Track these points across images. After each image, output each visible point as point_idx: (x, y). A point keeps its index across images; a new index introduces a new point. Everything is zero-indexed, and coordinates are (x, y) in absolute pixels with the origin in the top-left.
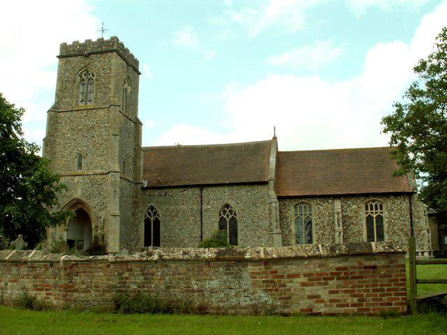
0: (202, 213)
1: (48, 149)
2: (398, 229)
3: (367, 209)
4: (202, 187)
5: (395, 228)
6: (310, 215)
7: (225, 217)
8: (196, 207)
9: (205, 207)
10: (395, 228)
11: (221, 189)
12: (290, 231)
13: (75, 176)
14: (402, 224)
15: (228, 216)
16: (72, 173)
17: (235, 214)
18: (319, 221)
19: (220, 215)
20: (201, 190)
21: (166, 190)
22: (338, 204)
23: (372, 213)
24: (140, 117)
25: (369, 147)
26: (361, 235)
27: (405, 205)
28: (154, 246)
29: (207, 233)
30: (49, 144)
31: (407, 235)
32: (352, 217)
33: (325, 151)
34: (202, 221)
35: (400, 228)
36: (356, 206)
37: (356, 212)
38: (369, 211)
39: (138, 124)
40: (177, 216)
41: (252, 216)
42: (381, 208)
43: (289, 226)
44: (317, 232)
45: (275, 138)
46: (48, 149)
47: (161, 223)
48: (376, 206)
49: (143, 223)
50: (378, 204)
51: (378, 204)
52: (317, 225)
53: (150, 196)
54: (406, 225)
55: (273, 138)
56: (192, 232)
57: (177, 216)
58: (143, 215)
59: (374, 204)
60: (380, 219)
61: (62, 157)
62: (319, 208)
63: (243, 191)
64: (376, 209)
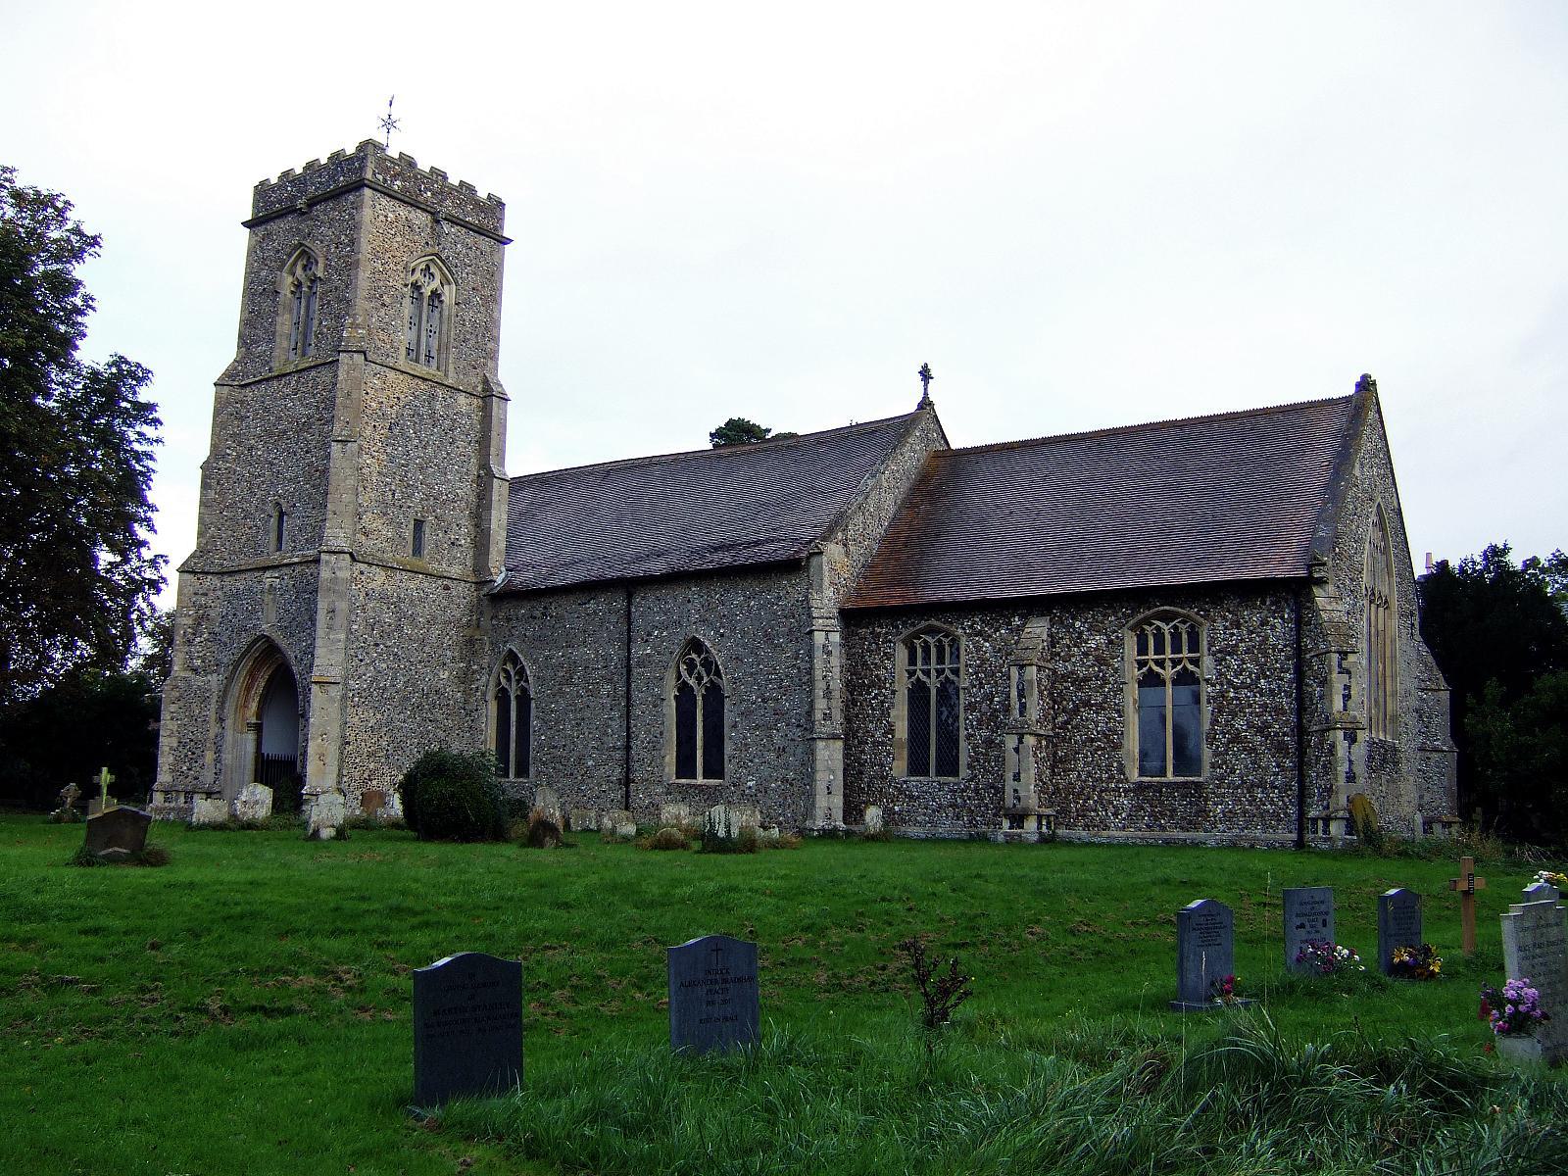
0: (629, 671)
1: (212, 494)
2: (1250, 725)
3: (1142, 649)
4: (629, 586)
5: (1240, 723)
6: (956, 672)
7: (692, 682)
8: (615, 652)
9: (639, 651)
10: (1240, 723)
11: (681, 593)
12: (890, 730)
13: (265, 569)
14: (1264, 706)
15: (699, 679)
16: (261, 561)
17: (718, 673)
18: (978, 694)
19: (679, 676)
20: (629, 597)
21: (545, 602)
22: (1038, 629)
23: (1161, 663)
24: (507, 375)
25: (978, 445)
26: (1117, 747)
27: (1279, 630)
28: (939, 773)
29: (642, 735)
30: (214, 482)
31: (1281, 748)
32: (1086, 679)
33: (1266, 412)
34: (629, 699)
35: (1257, 721)
36: (1101, 639)
37: (1101, 661)
38: (1151, 655)
39: (489, 397)
40: (569, 681)
41: (761, 679)
42: (1194, 646)
43: (886, 713)
44: (969, 737)
45: (926, 404)
46: (212, 494)
47: (533, 705)
48: (1176, 636)
49: (492, 707)
50: (1183, 628)
51: (1183, 628)
52: (971, 707)
53: (509, 620)
54: (1279, 711)
55: (921, 406)
56: (606, 734)
57: (569, 681)
58: (492, 684)
59: (1166, 628)
60: (948, 693)
61: (245, 518)
62: (978, 649)
63: (737, 598)
64: (1177, 649)
